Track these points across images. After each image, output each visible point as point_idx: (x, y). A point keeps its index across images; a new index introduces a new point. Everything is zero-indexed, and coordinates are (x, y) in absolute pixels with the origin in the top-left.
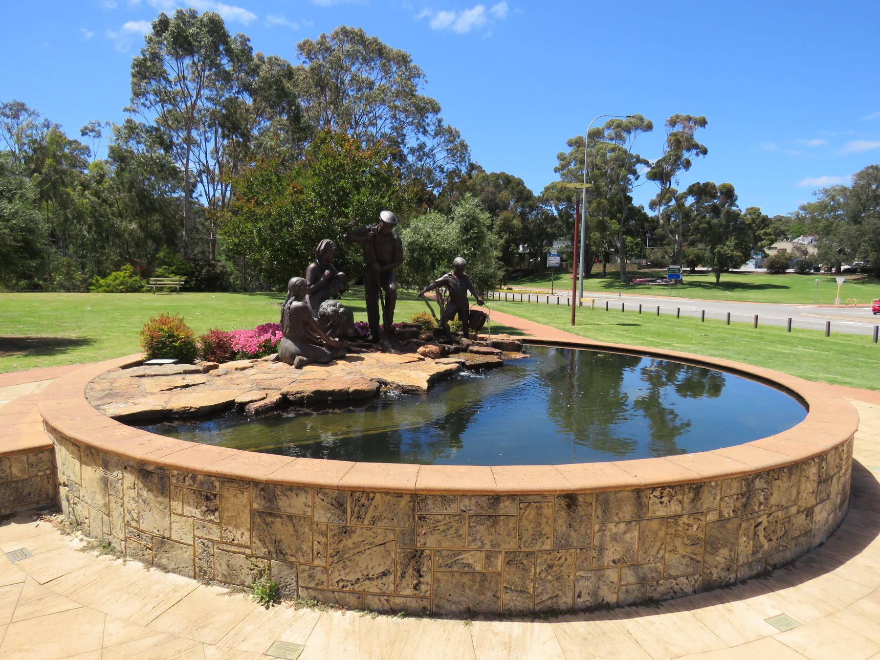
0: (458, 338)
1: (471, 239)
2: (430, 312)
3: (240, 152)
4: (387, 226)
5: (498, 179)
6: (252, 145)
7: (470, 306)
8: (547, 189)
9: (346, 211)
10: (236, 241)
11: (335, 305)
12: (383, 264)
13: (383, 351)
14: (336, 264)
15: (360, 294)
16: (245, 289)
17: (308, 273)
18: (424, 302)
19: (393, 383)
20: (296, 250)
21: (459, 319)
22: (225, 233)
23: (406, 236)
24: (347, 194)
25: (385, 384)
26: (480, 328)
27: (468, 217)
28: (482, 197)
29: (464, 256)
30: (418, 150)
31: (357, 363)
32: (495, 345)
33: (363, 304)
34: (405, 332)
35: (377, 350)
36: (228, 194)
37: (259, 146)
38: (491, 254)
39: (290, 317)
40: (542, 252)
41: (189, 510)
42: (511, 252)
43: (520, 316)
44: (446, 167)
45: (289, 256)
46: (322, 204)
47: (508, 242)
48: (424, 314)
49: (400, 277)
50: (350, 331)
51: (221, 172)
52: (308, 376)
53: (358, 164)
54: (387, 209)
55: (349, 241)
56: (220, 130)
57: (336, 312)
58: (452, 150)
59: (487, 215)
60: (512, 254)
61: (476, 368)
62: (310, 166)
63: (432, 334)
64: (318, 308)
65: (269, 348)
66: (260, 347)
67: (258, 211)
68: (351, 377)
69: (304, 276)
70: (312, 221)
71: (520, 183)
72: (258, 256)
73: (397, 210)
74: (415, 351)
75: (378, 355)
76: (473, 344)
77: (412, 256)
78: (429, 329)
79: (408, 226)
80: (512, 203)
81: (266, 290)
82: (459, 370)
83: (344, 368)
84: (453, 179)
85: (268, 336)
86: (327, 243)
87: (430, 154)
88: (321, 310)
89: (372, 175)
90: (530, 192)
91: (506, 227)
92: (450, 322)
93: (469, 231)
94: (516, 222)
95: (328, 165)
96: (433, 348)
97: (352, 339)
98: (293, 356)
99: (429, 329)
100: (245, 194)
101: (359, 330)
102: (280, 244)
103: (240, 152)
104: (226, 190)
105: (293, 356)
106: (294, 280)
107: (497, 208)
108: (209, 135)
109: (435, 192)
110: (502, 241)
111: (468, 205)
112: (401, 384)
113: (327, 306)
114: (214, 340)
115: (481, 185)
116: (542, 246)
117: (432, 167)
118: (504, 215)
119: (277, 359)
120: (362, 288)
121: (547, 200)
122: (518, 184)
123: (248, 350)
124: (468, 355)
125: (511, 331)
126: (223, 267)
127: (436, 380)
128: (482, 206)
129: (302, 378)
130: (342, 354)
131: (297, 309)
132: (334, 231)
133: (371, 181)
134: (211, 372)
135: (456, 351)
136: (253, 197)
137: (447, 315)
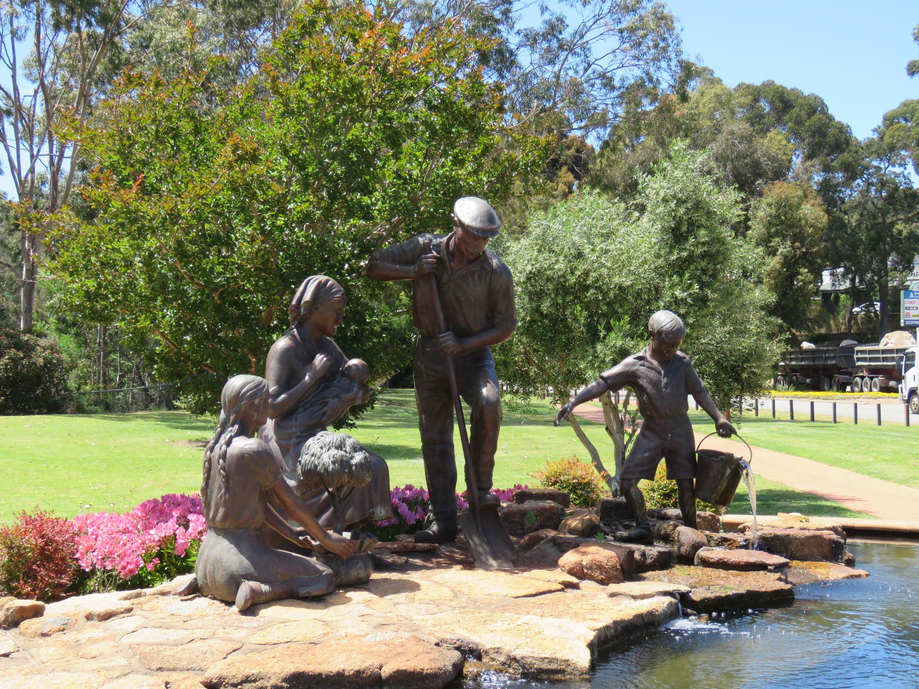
0: (666, 527)
1: (690, 259)
2: (587, 457)
3: (97, 61)
4: (474, 237)
5: (756, 100)
6: (126, 42)
7: (698, 437)
8: (890, 120)
9: (366, 200)
10: (91, 284)
11: (340, 447)
12: (462, 334)
13: (469, 564)
14: (342, 339)
15: (400, 412)
16: (106, 406)
17: (272, 363)
18: (569, 430)
19: (498, 651)
20: (239, 305)
21: (670, 477)
22: (64, 267)
23: (519, 257)
24: (368, 160)
25: (476, 653)
26: (725, 497)
27: (680, 202)
28: (715, 147)
29: (674, 305)
30: (545, 36)
31: (401, 597)
32: (770, 544)
33: (412, 438)
34: (523, 514)
35: (452, 562)
36: (66, 165)
37: (145, 44)
38: (747, 298)
39: (227, 478)
40: (884, 288)
41: (668, 326)
42: (801, 289)
43: (834, 462)
44: (618, 75)
45: (224, 320)
46: (306, 186)
47: (791, 264)
48: (574, 463)
49: (505, 364)
50: (381, 512)
51: (49, 115)
52: (273, 635)
53: (395, 81)
54: (471, 193)
55: (375, 277)
56: (49, 10)
57: (344, 464)
58: (632, 30)
59: (732, 195)
60: (804, 295)
61: (731, 608)
62: (276, 92)
63: (595, 518)
64: (298, 454)
65: (170, 561)
66: (148, 558)
67: (147, 208)
68: (387, 635)
69: (261, 372)
70: (281, 229)
71: (815, 107)
72: (144, 322)
73: (497, 193)
74: (553, 564)
75: (456, 575)
76: (709, 542)
77: (537, 310)
78: (587, 502)
79: (523, 229)
80: (797, 161)
81: (159, 406)
82: (672, 614)
83: (366, 610)
84: (638, 104)
85: (168, 527)
86: (321, 286)
87: (575, 46)
88: (305, 458)
89: (432, 108)
90: (843, 130)
91: (784, 224)
92: (643, 484)
93: (686, 239)
94: (812, 212)
95: (320, 88)
96: (600, 554)
97: (387, 533)
98: (234, 582)
99: (587, 502)
100: (114, 168)
101: (404, 508)
102: (202, 289)
103: (97, 61)
104: (61, 157)
105: (234, 582)
106: (237, 382)
107: (759, 176)
108: (21, 22)
109: (593, 141)
110: (774, 262)
111: (683, 172)
112: (518, 654)
113: (322, 448)
114: (31, 542)
115: (711, 118)
116: (882, 272)
117: (580, 78)
118: (775, 192)
119: (194, 590)
120: (410, 396)
121: (892, 148)
122: (812, 111)
123: (117, 566)
124: (696, 572)
125: (812, 504)
126: (52, 348)
127: (611, 644)
128: (719, 173)
129: (258, 638)
130: (362, 574)
131: (243, 459)
132: (334, 252)
133: (429, 125)
134: (24, 624)
135: (664, 563)
136: (134, 176)
137: (634, 468)
